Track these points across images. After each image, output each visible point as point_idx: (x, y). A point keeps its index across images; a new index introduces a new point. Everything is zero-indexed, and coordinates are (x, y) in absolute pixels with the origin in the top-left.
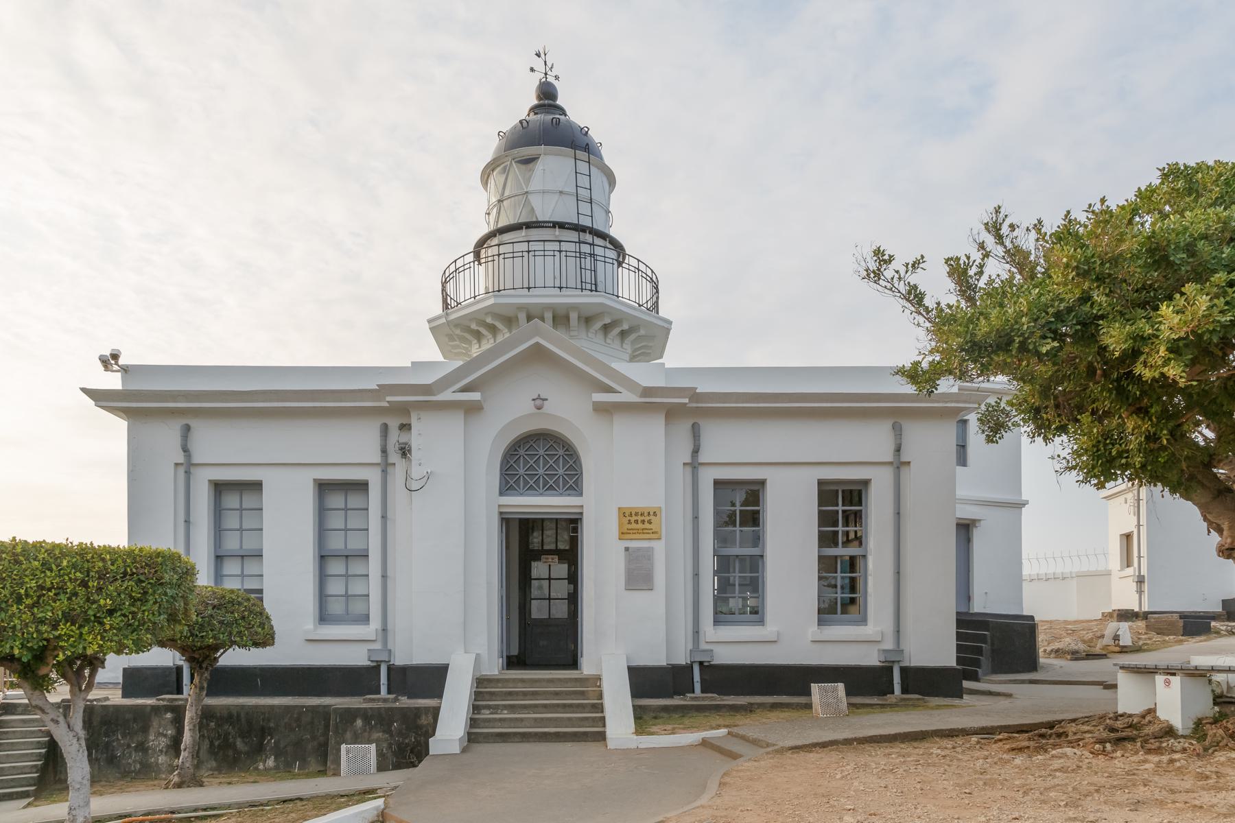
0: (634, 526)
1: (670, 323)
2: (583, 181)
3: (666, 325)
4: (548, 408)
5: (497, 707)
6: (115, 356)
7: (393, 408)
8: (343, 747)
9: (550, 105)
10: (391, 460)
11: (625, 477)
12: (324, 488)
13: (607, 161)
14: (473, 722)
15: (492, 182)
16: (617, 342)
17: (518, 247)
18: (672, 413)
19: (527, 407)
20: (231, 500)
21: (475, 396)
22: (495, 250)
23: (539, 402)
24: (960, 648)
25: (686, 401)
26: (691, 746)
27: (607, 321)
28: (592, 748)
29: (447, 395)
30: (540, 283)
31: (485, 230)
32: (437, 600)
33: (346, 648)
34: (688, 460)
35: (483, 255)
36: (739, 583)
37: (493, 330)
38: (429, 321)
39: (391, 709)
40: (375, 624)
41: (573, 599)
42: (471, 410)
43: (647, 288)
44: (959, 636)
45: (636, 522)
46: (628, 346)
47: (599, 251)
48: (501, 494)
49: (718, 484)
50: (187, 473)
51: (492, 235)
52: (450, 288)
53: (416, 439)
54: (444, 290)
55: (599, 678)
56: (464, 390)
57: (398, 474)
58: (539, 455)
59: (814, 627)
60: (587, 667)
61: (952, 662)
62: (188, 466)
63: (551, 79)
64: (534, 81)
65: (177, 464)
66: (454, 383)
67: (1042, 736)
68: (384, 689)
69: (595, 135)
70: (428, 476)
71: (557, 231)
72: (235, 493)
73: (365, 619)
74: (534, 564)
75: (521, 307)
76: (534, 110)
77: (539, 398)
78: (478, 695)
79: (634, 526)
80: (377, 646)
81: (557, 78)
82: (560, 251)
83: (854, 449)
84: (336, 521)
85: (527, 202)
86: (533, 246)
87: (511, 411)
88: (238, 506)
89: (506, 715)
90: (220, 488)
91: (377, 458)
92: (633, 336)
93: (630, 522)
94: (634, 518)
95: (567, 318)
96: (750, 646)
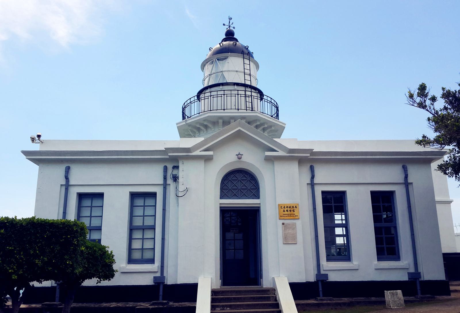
0: (286, 213)
2: (247, 67)
3: (283, 125)
4: (244, 159)
9: (231, 38)
11: (281, 191)
12: (134, 196)
18: (301, 161)
19: (234, 158)
20: (87, 202)
22: (209, 94)
23: (239, 156)
25: (309, 155)
27: (258, 123)
29: (197, 153)
31: (202, 87)
33: (141, 276)
37: (206, 127)
38: (177, 124)
40: (155, 266)
42: (208, 159)
45: (289, 212)
48: (221, 198)
49: (323, 192)
50: (67, 190)
56: (206, 150)
59: (376, 262)
60: (266, 284)
62: (67, 186)
63: (232, 28)
64: (224, 30)
65: (61, 185)
66: (201, 147)
68: (161, 297)
69: (251, 49)
70: (187, 190)
71: (236, 87)
72: (91, 199)
73: (152, 261)
75: (221, 118)
76: (225, 40)
77: (239, 154)
78: (213, 300)
79: (286, 213)
80: (158, 275)
81: (234, 28)
82: (224, 95)
84: (139, 212)
87: (226, 160)
88: (90, 205)
90: (81, 196)
91: (161, 182)
92: (268, 131)
93: (284, 211)
94: (286, 209)
96: (343, 272)
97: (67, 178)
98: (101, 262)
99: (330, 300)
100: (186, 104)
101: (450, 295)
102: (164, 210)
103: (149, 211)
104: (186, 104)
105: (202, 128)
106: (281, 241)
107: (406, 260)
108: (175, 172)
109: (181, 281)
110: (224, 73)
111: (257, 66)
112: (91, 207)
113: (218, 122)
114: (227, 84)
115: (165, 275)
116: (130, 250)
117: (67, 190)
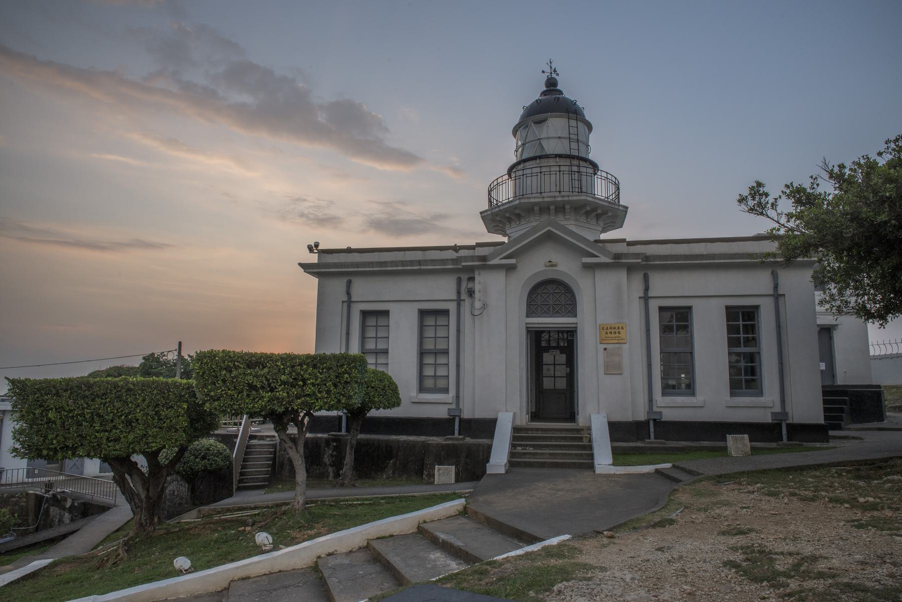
1: (627, 208)
5: (527, 445)
6: (317, 245)
7: (464, 266)
8: (437, 467)
10: (462, 298)
11: (605, 309)
12: (423, 313)
13: (587, 118)
14: (512, 455)
15: (518, 133)
16: (594, 221)
17: (535, 170)
18: (631, 269)
20: (371, 321)
21: (513, 261)
22: (521, 173)
24: (826, 410)
26: (648, 473)
28: (587, 473)
30: (547, 190)
32: (492, 379)
33: (436, 407)
34: (642, 295)
35: (513, 175)
36: (678, 371)
38: (481, 213)
39: (462, 444)
40: (450, 396)
41: (571, 378)
42: (510, 269)
43: (612, 189)
44: (825, 402)
45: (611, 333)
46: (601, 223)
47: (582, 169)
48: (527, 316)
49: (662, 309)
50: (349, 307)
51: (518, 163)
52: (494, 194)
53: (477, 287)
54: (489, 194)
55: (589, 429)
56: (505, 258)
57: (466, 306)
58: (551, 293)
59: (728, 398)
60: (581, 421)
61: (822, 421)
62: (349, 302)
63: (554, 76)
64: (544, 77)
67: (880, 468)
68: (456, 432)
71: (558, 159)
72: (375, 317)
73: (446, 390)
74: (544, 354)
76: (544, 93)
78: (514, 438)
79: (609, 335)
80: (453, 406)
83: (750, 286)
84: (430, 333)
85: (540, 143)
86: (544, 169)
87: (535, 266)
89: (531, 450)
90: (365, 314)
91: (454, 297)
95: (564, 208)
97: (348, 294)
98: (388, 392)
99: (661, 443)
100: (500, 180)
101: (828, 442)
102: (458, 331)
103: (441, 333)
104: (500, 180)
105: (513, 217)
106: (602, 370)
107: (770, 396)
108: (470, 285)
109: (479, 415)
110: (542, 142)
111: (589, 127)
112: (377, 326)
113: (533, 209)
114: (547, 156)
115: (461, 407)
116: (421, 377)
117: (349, 307)
